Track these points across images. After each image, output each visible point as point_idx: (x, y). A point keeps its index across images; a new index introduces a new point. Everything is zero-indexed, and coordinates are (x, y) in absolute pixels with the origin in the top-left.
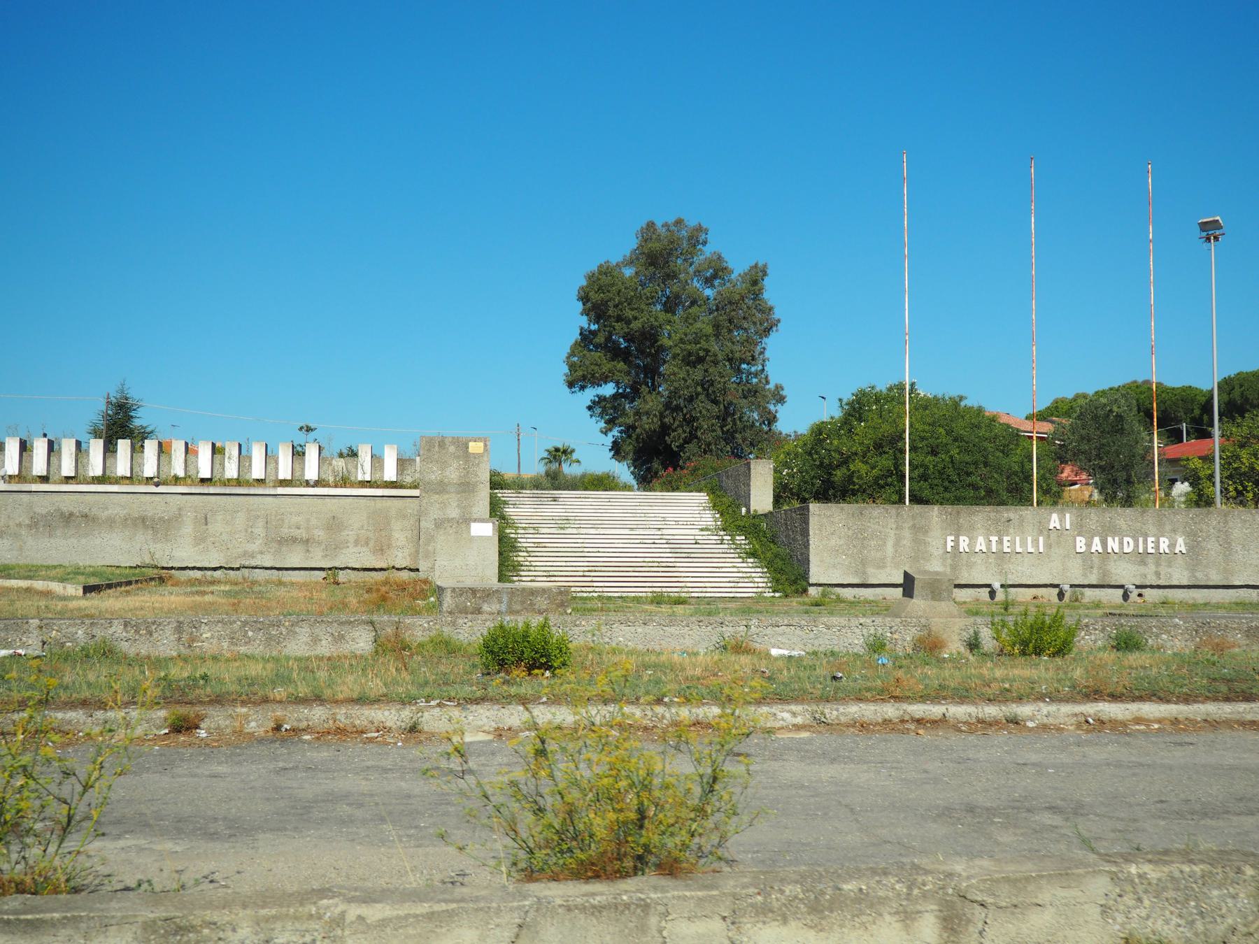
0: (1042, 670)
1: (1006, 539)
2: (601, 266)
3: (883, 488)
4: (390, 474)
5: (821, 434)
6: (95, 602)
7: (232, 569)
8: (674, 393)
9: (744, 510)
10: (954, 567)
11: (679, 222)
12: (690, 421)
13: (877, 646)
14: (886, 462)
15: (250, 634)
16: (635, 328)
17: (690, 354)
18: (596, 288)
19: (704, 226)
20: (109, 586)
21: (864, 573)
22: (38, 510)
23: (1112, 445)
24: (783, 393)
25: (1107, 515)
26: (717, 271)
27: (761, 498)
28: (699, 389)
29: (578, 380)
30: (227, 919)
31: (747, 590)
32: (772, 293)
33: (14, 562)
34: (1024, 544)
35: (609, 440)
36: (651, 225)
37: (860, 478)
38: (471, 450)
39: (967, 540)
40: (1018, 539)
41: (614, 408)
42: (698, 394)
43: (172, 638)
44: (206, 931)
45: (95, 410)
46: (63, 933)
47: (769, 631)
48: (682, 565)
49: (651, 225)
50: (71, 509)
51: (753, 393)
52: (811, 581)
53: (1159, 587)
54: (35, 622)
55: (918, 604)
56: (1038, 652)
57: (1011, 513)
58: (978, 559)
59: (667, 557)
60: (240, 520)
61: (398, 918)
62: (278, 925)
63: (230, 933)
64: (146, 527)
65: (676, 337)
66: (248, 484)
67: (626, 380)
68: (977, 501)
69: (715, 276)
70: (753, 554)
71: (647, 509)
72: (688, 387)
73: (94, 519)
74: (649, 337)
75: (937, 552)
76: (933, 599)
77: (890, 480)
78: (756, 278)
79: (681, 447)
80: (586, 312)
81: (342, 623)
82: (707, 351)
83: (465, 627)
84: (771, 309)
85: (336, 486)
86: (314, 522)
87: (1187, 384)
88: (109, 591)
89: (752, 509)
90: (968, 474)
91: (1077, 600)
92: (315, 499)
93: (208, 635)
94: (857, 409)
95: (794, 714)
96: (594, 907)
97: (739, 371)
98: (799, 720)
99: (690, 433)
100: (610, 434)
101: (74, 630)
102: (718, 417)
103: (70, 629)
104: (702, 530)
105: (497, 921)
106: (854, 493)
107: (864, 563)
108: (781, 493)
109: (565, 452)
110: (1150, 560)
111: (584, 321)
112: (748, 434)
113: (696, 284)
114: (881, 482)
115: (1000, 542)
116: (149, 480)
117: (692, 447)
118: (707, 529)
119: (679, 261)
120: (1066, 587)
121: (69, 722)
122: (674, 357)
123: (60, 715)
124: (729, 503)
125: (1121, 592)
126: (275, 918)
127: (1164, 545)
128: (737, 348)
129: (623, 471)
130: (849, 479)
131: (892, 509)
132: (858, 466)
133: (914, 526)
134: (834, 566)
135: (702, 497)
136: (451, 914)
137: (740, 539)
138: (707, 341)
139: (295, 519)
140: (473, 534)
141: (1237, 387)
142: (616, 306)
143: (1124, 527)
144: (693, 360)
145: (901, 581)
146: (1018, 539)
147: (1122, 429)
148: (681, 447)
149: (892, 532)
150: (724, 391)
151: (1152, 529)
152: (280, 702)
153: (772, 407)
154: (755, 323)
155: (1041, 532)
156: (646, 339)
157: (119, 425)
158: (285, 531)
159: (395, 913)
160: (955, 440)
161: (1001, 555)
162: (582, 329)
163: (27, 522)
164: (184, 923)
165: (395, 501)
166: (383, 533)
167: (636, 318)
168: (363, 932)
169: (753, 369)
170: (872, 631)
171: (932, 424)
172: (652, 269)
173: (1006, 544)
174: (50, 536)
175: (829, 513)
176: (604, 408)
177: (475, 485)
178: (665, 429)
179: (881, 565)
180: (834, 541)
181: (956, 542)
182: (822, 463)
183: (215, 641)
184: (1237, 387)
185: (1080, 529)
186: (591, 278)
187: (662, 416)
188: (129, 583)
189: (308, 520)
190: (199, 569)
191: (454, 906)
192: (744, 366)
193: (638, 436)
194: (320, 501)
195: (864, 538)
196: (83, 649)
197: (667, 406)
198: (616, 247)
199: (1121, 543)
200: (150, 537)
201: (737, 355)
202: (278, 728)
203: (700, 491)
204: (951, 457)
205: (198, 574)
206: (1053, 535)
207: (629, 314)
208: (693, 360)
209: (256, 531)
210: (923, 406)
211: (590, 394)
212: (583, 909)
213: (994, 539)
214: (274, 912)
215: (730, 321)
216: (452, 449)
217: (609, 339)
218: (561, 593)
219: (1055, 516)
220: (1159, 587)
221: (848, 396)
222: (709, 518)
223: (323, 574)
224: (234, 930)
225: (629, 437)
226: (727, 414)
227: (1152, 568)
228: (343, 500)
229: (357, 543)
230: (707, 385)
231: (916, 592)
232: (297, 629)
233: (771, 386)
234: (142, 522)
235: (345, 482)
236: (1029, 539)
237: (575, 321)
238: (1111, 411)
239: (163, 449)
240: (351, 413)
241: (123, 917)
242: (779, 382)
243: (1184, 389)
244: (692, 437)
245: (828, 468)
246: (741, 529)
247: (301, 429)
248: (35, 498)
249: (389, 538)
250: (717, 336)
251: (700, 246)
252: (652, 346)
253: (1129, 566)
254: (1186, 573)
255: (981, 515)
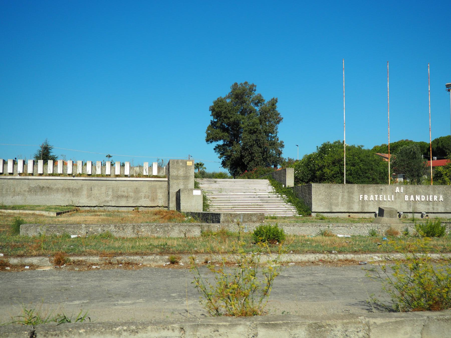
0: (432, 242)
1: (380, 196)
2: (218, 98)
3: (336, 178)
4: (155, 173)
5: (310, 158)
6: (62, 218)
7: (101, 207)
8: (245, 144)
9: (283, 186)
10: (363, 206)
11: (246, 83)
12: (251, 154)
13: (373, 234)
14: (336, 169)
15: (158, 229)
16: (232, 121)
17: (251, 130)
18: (217, 106)
19: (255, 84)
20: (64, 213)
21: (331, 208)
22: (31, 185)
23: (411, 162)
24: (283, 144)
25: (416, 187)
26: (259, 101)
27: (290, 182)
28: (254, 142)
29: (210, 139)
30: (334, 323)
31: (290, 214)
32: (279, 108)
33: (24, 204)
34: (387, 197)
35: (221, 161)
36: (236, 84)
37: (327, 174)
38: (188, 164)
39: (407, 196)
40: (385, 196)
41: (224, 149)
42: (254, 144)
43: (131, 231)
44: (327, 327)
45: (37, 149)
46: (284, 328)
47: (336, 228)
48: (265, 205)
49: (236, 84)
50: (43, 185)
51: (273, 144)
52: (313, 211)
53: (434, 213)
54: (83, 226)
55: (385, 219)
56: (433, 235)
57: (382, 187)
58: (371, 203)
59: (260, 203)
60: (104, 189)
61: (386, 323)
62: (350, 325)
63: (335, 328)
64: (70, 192)
65: (246, 124)
66: (26, 175)
67: (228, 139)
68: (369, 183)
69: (259, 102)
70: (290, 201)
71: (248, 185)
72: (250, 142)
73: (52, 189)
74: (236, 124)
75: (356, 201)
76: (390, 217)
77: (338, 175)
78: (273, 103)
79: (248, 163)
80: (212, 115)
81: (189, 226)
82: (257, 129)
83: (232, 227)
84: (279, 114)
85: (137, 177)
86: (129, 190)
87: (422, 141)
88: (64, 214)
89: (287, 186)
90: (366, 173)
91: (405, 218)
92: (130, 182)
93: (144, 230)
94: (324, 150)
95: (379, 257)
96: (446, 319)
97: (268, 136)
98: (380, 259)
99: (251, 158)
100: (222, 158)
101: (97, 228)
102: (261, 153)
103: (96, 228)
104: (269, 193)
105: (417, 324)
106: (325, 180)
107: (331, 204)
108: (297, 180)
109: (201, 165)
110: (431, 203)
111: (212, 118)
112: (272, 158)
113: (252, 105)
114: (335, 176)
115: (379, 197)
116: (69, 175)
117: (252, 163)
118: (271, 193)
119: (246, 97)
120: (402, 213)
121: (136, 260)
122: (245, 131)
123: (132, 258)
124: (277, 182)
125: (420, 215)
126: (349, 323)
127: (436, 198)
128: (267, 128)
129: (226, 171)
130: (323, 175)
131: (341, 185)
132: (326, 170)
133: (348, 191)
134: (321, 206)
135: (267, 181)
136: (402, 322)
137: (284, 196)
138: (257, 125)
139: (123, 189)
140: (194, 194)
141: (440, 142)
142: (224, 113)
143: (422, 192)
144: (252, 132)
145: (212, 210)
146: (385, 196)
147: (416, 157)
148: (248, 163)
149: (341, 194)
150: (264, 143)
151: (431, 192)
152: (202, 253)
153: (280, 149)
154: (274, 119)
155: (393, 194)
156: (235, 124)
157: (45, 155)
158: (119, 193)
159: (385, 321)
160: (361, 161)
161: (379, 201)
162: (211, 121)
163: (28, 190)
164: (321, 324)
165: (159, 182)
166: (154, 194)
167: (232, 117)
168: (376, 328)
169: (273, 135)
170: (371, 228)
171: (353, 155)
172: (237, 100)
173: (381, 198)
174: (36, 195)
175: (319, 187)
176: (220, 150)
177: (189, 177)
178: (242, 157)
179: (337, 205)
180: (320, 197)
181: (363, 197)
182: (311, 169)
183: (146, 232)
184: (440, 142)
185: (406, 192)
186: (216, 103)
187: (241, 152)
188: (68, 212)
189: (127, 189)
190: (89, 207)
191: (403, 319)
192: (270, 134)
193: (232, 159)
194: (131, 182)
195: (331, 196)
196: (101, 235)
197: (243, 148)
198: (224, 91)
199: (421, 197)
200: (71, 195)
201: (268, 130)
202: (206, 262)
203: (266, 179)
204: (360, 167)
205: (89, 208)
206: (397, 195)
207: (229, 115)
208: (252, 132)
209: (109, 193)
210: (349, 149)
211: (215, 144)
212: (442, 320)
213: (376, 196)
214: (348, 321)
215: (265, 118)
216: (181, 164)
217: (221, 125)
218: (261, 215)
219: (397, 188)
220: (434, 213)
221: (320, 146)
222: (271, 189)
223: (134, 208)
224: (336, 327)
225: (229, 159)
226: (265, 152)
227: (431, 206)
228: (140, 182)
229: (145, 197)
230: (257, 141)
231: (384, 215)
232: (174, 228)
233: (279, 141)
234: (68, 190)
235: (139, 176)
236: (389, 196)
237: (209, 118)
238: (411, 151)
239: (64, 164)
240: (125, 150)
241: (302, 323)
242: (282, 140)
243: (421, 143)
244: (252, 159)
245: (314, 171)
246: (285, 193)
247: (107, 156)
248: (30, 181)
249: (156, 195)
250: (261, 124)
251: (253, 92)
252: (237, 127)
253: (423, 206)
254: (443, 208)
255: (372, 188)
